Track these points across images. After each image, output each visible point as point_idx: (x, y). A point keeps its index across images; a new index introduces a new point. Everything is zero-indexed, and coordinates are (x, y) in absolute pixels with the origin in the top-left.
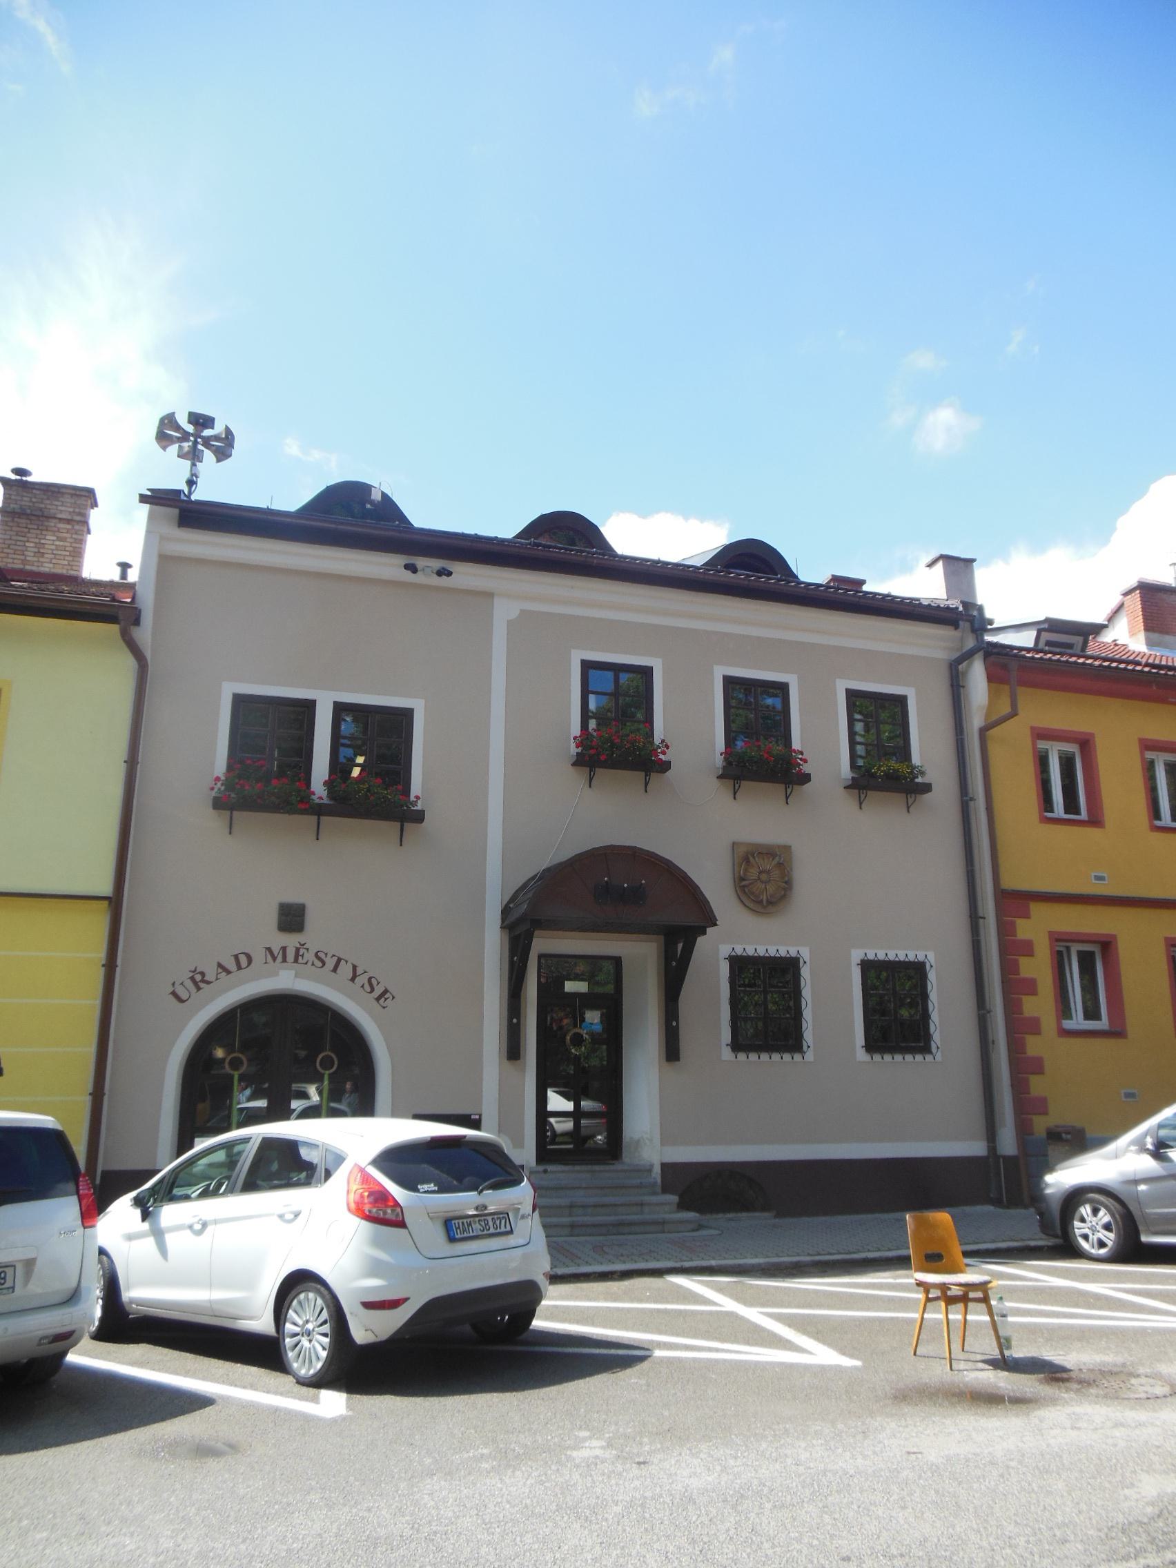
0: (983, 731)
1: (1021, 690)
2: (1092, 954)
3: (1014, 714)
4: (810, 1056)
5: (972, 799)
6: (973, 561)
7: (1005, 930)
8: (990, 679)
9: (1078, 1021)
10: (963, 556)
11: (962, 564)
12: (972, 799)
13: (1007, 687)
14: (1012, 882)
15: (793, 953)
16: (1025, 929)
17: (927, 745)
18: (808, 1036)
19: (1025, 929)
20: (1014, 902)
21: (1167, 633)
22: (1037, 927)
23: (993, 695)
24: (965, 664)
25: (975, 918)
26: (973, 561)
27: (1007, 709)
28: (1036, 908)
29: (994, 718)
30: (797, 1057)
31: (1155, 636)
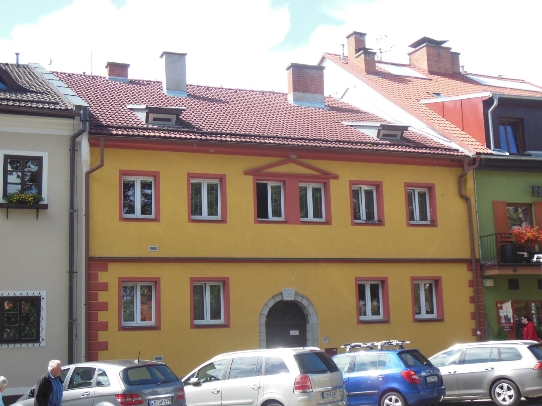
0: (88, 174)
1: (106, 150)
2: (377, 285)
3: (101, 166)
4: (43, 344)
5: (75, 211)
6: (185, 55)
7: (90, 278)
8: (92, 145)
9: (208, 320)
10: (178, 52)
11: (178, 57)
12: (75, 211)
13: (98, 149)
14: (96, 253)
15: (36, 294)
16: (103, 277)
17: (53, 186)
18: (43, 334)
19: (103, 277)
20: (96, 263)
21: (308, 92)
22: (110, 276)
23: (92, 153)
24: (80, 137)
25: (72, 272)
26: (185, 55)
27: (98, 163)
28: (111, 266)
29: (93, 167)
30: (37, 345)
31: (300, 94)
